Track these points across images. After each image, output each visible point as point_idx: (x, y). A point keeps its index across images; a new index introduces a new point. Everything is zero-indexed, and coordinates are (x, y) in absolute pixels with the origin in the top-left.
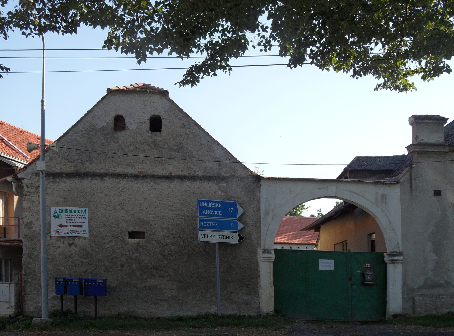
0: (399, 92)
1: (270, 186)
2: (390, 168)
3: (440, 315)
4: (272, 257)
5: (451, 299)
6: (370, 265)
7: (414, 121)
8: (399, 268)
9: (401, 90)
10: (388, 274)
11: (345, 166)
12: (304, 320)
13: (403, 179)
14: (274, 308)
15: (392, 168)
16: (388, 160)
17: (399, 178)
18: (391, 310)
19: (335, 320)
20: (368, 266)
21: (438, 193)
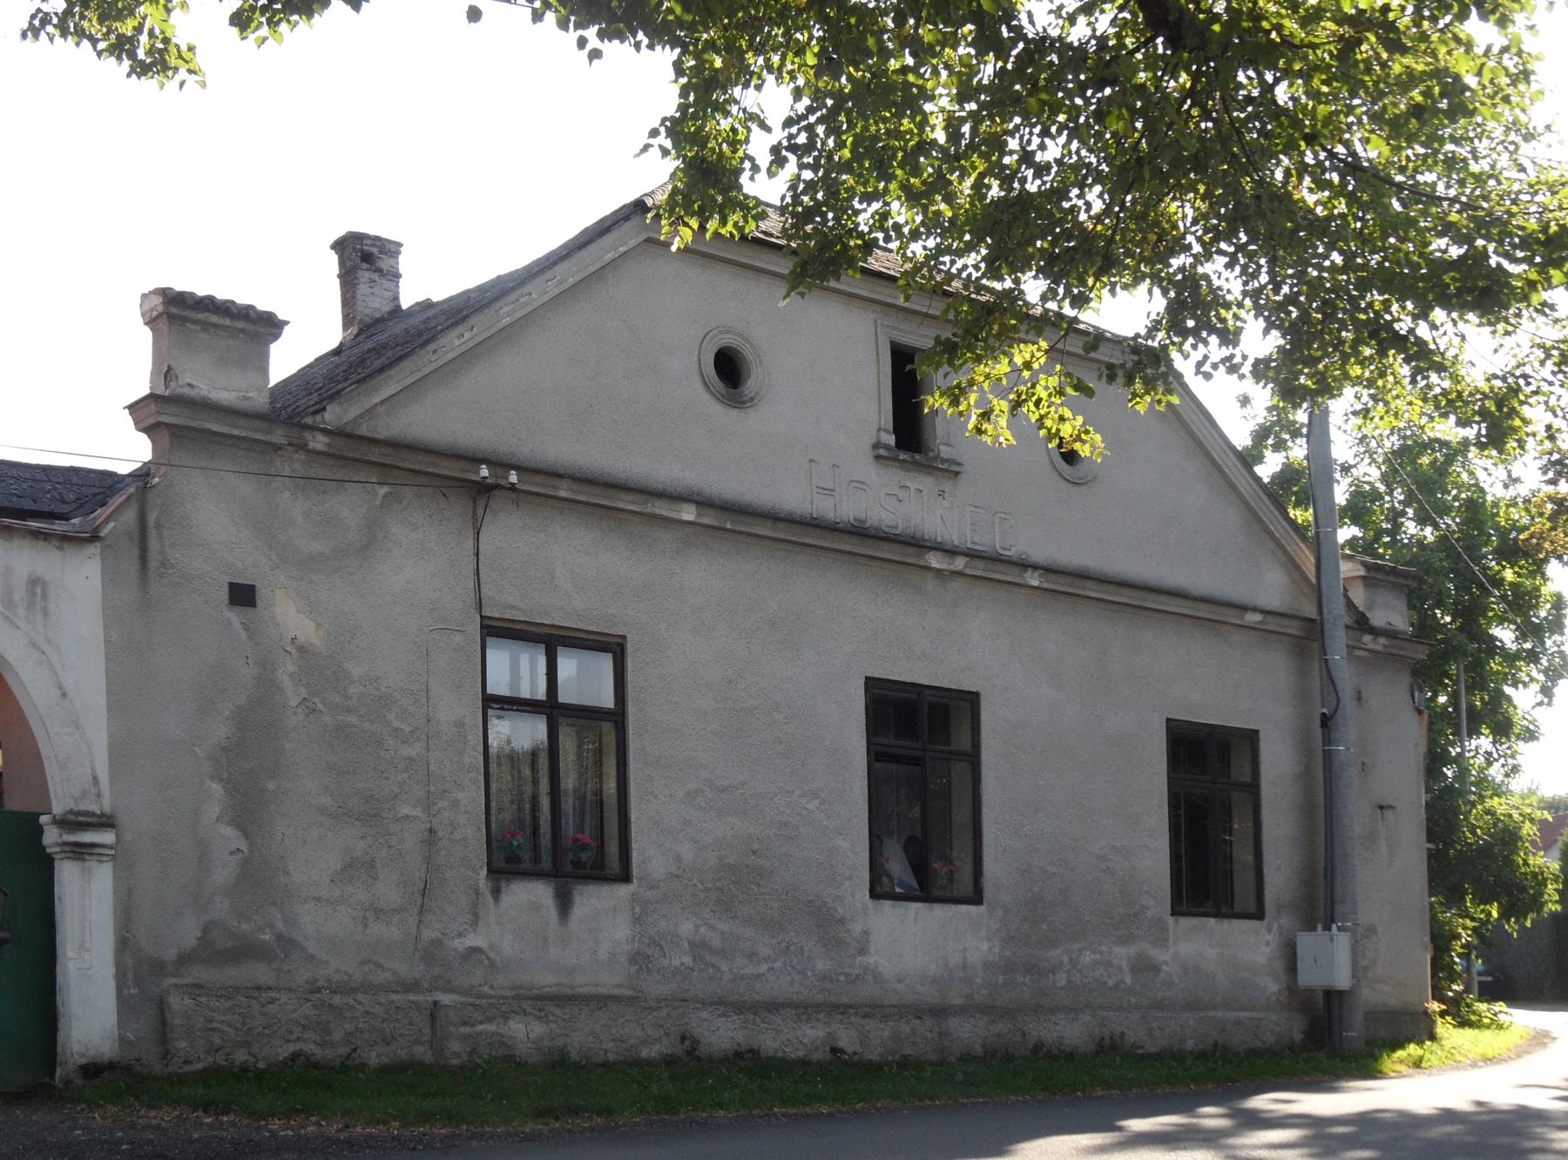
0: (129, 75)
3: (261, 1065)
5: (301, 1005)
7: (160, 309)
8: (103, 877)
9: (141, 69)
13: (111, 525)
17: (98, 522)
18: (76, 1048)
21: (243, 595)
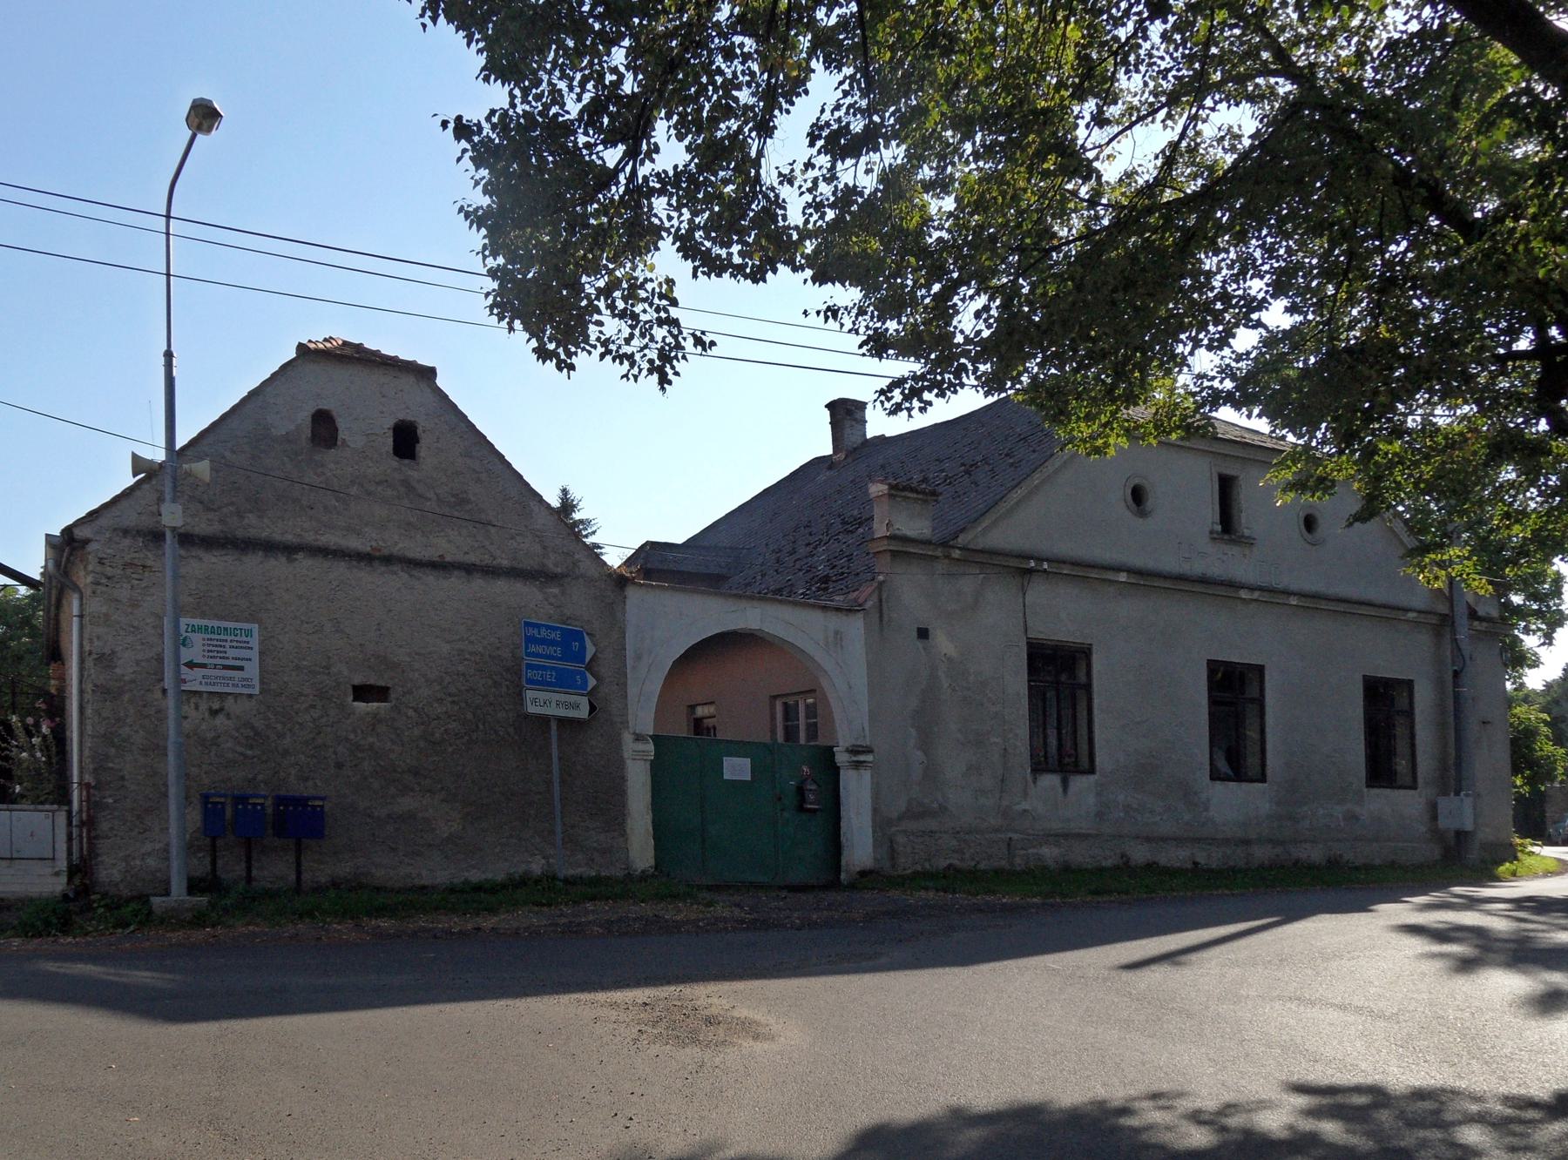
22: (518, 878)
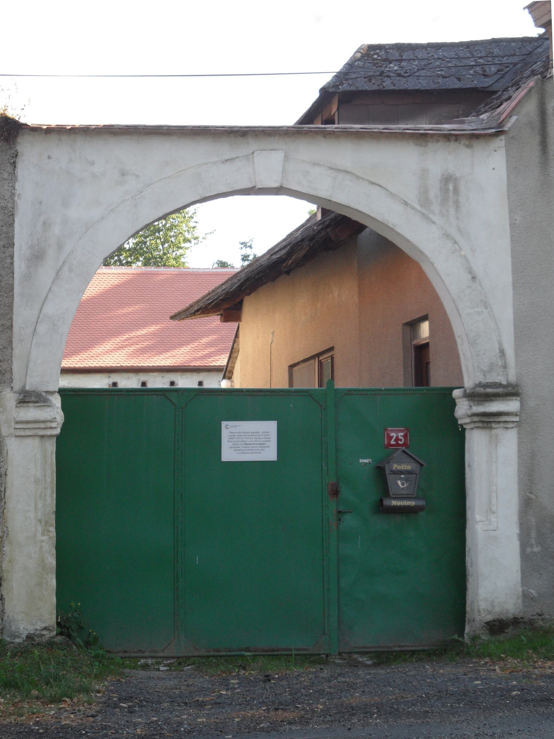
1: (49, 157)
2: (476, 83)
4: (53, 420)
6: (405, 436)
10: (469, 466)
11: (326, 79)
12: (168, 658)
13: (514, 118)
14: (54, 617)
15: (486, 83)
16: (475, 54)
18: (483, 605)
19: (278, 650)
20: (397, 439)
22: (13, 628)
